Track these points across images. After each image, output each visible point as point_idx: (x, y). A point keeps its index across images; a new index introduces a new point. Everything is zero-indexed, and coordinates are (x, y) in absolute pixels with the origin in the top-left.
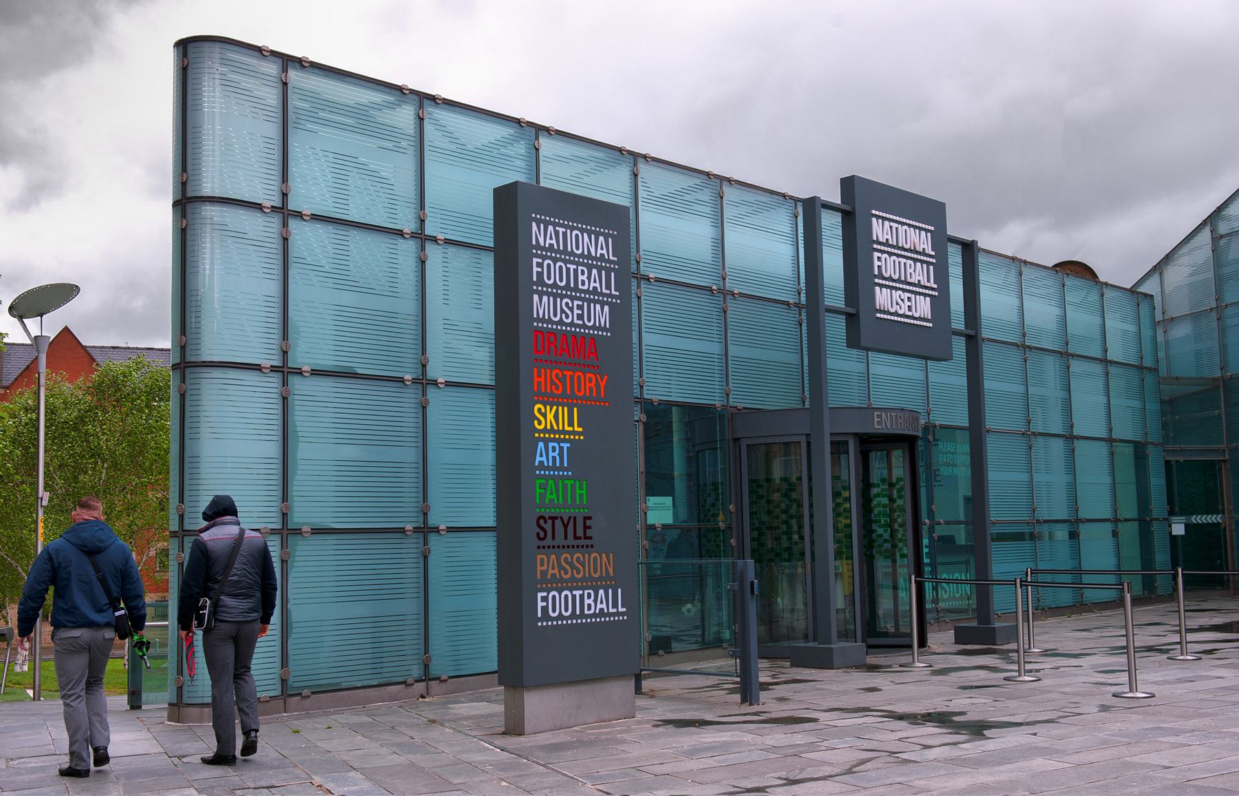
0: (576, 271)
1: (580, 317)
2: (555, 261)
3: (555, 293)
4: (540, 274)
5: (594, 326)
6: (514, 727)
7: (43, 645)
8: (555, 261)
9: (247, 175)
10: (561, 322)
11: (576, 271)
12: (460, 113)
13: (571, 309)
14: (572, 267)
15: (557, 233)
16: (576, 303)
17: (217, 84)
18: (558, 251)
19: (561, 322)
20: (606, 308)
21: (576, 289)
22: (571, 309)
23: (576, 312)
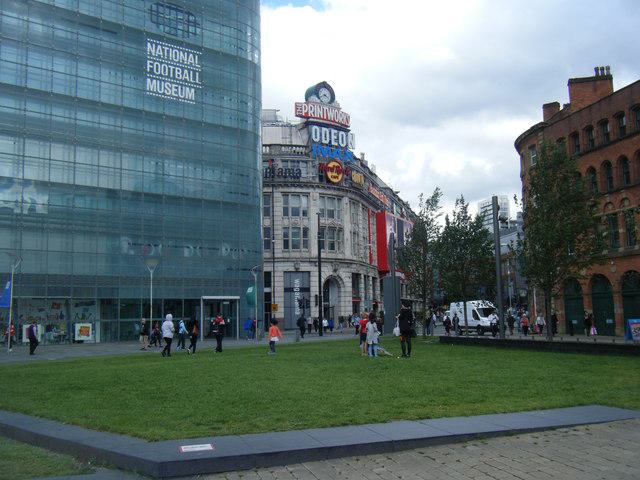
0: (174, 70)
1: (176, 93)
2: (161, 63)
3: (160, 78)
4: (152, 69)
5: (184, 99)
6: (219, 349)
7: (98, 341)
8: (161, 63)
9: (374, 291)
10: (164, 94)
11: (174, 70)
12: (11, 94)
13: (171, 88)
14: (172, 68)
15: (163, 50)
16: (174, 85)
17: (332, 256)
18: (166, 77)
19: (164, 94)
20: (193, 90)
21: (174, 78)
22: (171, 88)
23: (174, 90)
